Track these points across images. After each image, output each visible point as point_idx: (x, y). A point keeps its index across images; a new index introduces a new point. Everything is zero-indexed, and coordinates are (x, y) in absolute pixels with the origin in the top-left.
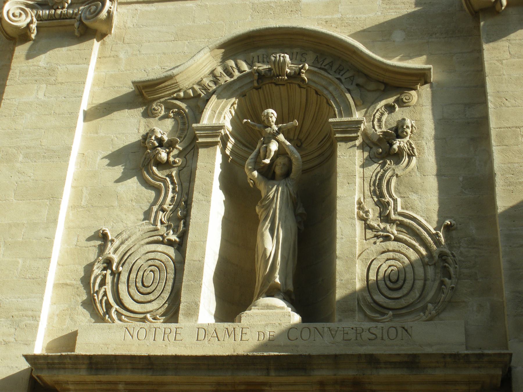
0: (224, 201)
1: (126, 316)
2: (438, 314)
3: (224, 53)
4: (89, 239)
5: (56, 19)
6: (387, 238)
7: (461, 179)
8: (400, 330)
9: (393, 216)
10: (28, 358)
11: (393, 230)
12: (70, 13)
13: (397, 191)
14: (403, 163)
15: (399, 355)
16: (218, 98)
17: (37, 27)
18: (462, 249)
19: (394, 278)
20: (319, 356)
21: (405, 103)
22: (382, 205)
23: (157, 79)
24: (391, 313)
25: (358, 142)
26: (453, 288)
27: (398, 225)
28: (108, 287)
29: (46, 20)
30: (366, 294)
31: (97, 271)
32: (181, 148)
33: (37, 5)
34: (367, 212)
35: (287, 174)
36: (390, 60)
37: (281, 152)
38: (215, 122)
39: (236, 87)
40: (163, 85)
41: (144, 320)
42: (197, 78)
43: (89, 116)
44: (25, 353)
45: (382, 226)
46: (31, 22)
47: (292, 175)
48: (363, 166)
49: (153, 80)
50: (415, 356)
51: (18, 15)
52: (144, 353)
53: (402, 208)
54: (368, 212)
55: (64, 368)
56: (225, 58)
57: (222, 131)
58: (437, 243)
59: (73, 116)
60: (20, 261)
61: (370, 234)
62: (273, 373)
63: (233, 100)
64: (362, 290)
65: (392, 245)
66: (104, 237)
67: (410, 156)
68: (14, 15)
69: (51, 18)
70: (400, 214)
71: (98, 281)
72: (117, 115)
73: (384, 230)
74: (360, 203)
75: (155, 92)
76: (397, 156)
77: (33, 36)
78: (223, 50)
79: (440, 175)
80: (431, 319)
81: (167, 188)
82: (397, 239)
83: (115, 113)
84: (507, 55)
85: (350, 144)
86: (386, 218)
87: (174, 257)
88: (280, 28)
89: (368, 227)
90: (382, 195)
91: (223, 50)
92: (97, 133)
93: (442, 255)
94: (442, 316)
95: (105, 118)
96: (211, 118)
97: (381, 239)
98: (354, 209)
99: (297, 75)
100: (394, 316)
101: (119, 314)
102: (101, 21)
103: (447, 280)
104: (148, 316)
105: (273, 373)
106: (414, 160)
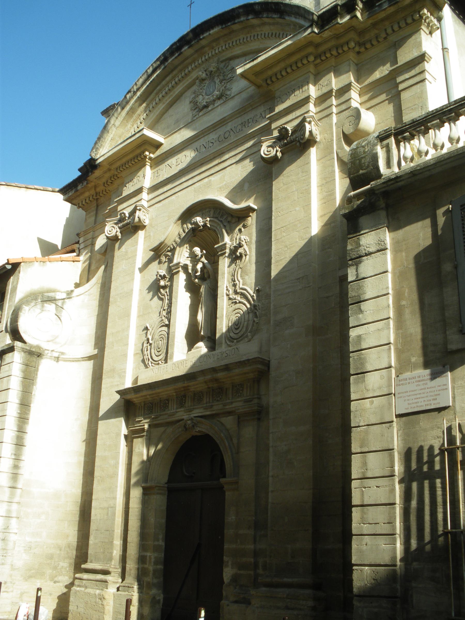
0: (190, 297)
1: (154, 364)
2: (252, 337)
3: (181, 222)
4: (143, 331)
5: (125, 226)
6: (236, 303)
7: (265, 262)
8: (236, 349)
9: (238, 291)
10: (118, 392)
11: (238, 298)
12: (285, 143)
13: (241, 276)
14: (245, 261)
15: (221, 366)
16: (180, 247)
17: (121, 232)
18: (263, 301)
19: (237, 323)
20: (197, 372)
21: (246, 225)
22: (235, 285)
23: (157, 246)
24: (235, 341)
25: (227, 255)
26: (257, 323)
27: (240, 295)
28: (149, 352)
29: (123, 228)
30: (228, 334)
31: (145, 345)
32: (169, 277)
33: (119, 222)
34: (229, 291)
35: (209, 277)
36: (240, 205)
37: (204, 267)
38: (179, 261)
39: (186, 238)
40: (161, 247)
41: (158, 364)
42: (172, 240)
43: (141, 270)
44: (117, 390)
45: (234, 296)
46: (117, 232)
47: (211, 277)
48: (229, 266)
49: (156, 247)
50: (227, 365)
51: (111, 230)
52: (146, 383)
53: (243, 285)
54: (229, 291)
55: (128, 394)
56: (182, 224)
57: (181, 264)
58: (253, 300)
59: (133, 272)
60: (120, 348)
61: (230, 301)
62: (186, 382)
63: (186, 246)
64: (226, 332)
65: (238, 306)
66: (146, 329)
67: (246, 255)
68: (110, 231)
69: (124, 226)
70: (242, 289)
71: (146, 349)
72: (150, 266)
73: (235, 299)
74: (227, 287)
75: (160, 251)
76: (240, 257)
77: (120, 237)
78: (180, 221)
79: (257, 263)
80: (249, 341)
81: (165, 298)
82: (240, 302)
83: (150, 265)
84: (282, 185)
85: (224, 256)
86: (236, 293)
87: (167, 332)
88: (197, 202)
89: (230, 299)
90: (235, 281)
91: (180, 221)
92: (144, 278)
93: (255, 306)
94: (254, 338)
95: (147, 269)
96: (177, 258)
97: (234, 304)
98: (223, 291)
99: (205, 226)
100: (237, 342)
101: (152, 363)
102: (137, 222)
103: (255, 319)
104: (160, 362)
105: (186, 382)
106: (248, 257)
